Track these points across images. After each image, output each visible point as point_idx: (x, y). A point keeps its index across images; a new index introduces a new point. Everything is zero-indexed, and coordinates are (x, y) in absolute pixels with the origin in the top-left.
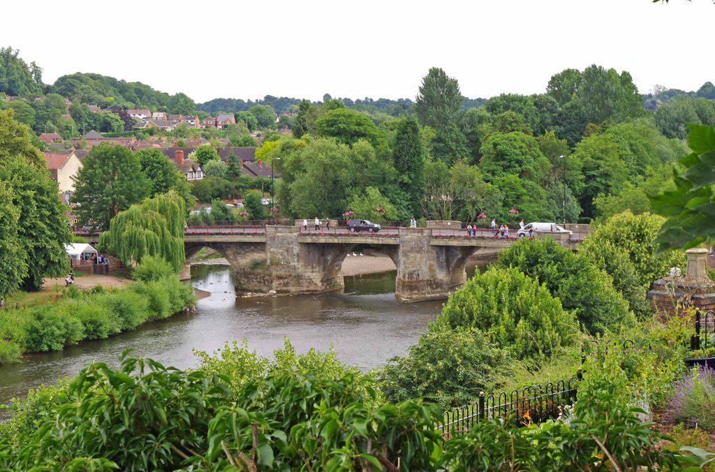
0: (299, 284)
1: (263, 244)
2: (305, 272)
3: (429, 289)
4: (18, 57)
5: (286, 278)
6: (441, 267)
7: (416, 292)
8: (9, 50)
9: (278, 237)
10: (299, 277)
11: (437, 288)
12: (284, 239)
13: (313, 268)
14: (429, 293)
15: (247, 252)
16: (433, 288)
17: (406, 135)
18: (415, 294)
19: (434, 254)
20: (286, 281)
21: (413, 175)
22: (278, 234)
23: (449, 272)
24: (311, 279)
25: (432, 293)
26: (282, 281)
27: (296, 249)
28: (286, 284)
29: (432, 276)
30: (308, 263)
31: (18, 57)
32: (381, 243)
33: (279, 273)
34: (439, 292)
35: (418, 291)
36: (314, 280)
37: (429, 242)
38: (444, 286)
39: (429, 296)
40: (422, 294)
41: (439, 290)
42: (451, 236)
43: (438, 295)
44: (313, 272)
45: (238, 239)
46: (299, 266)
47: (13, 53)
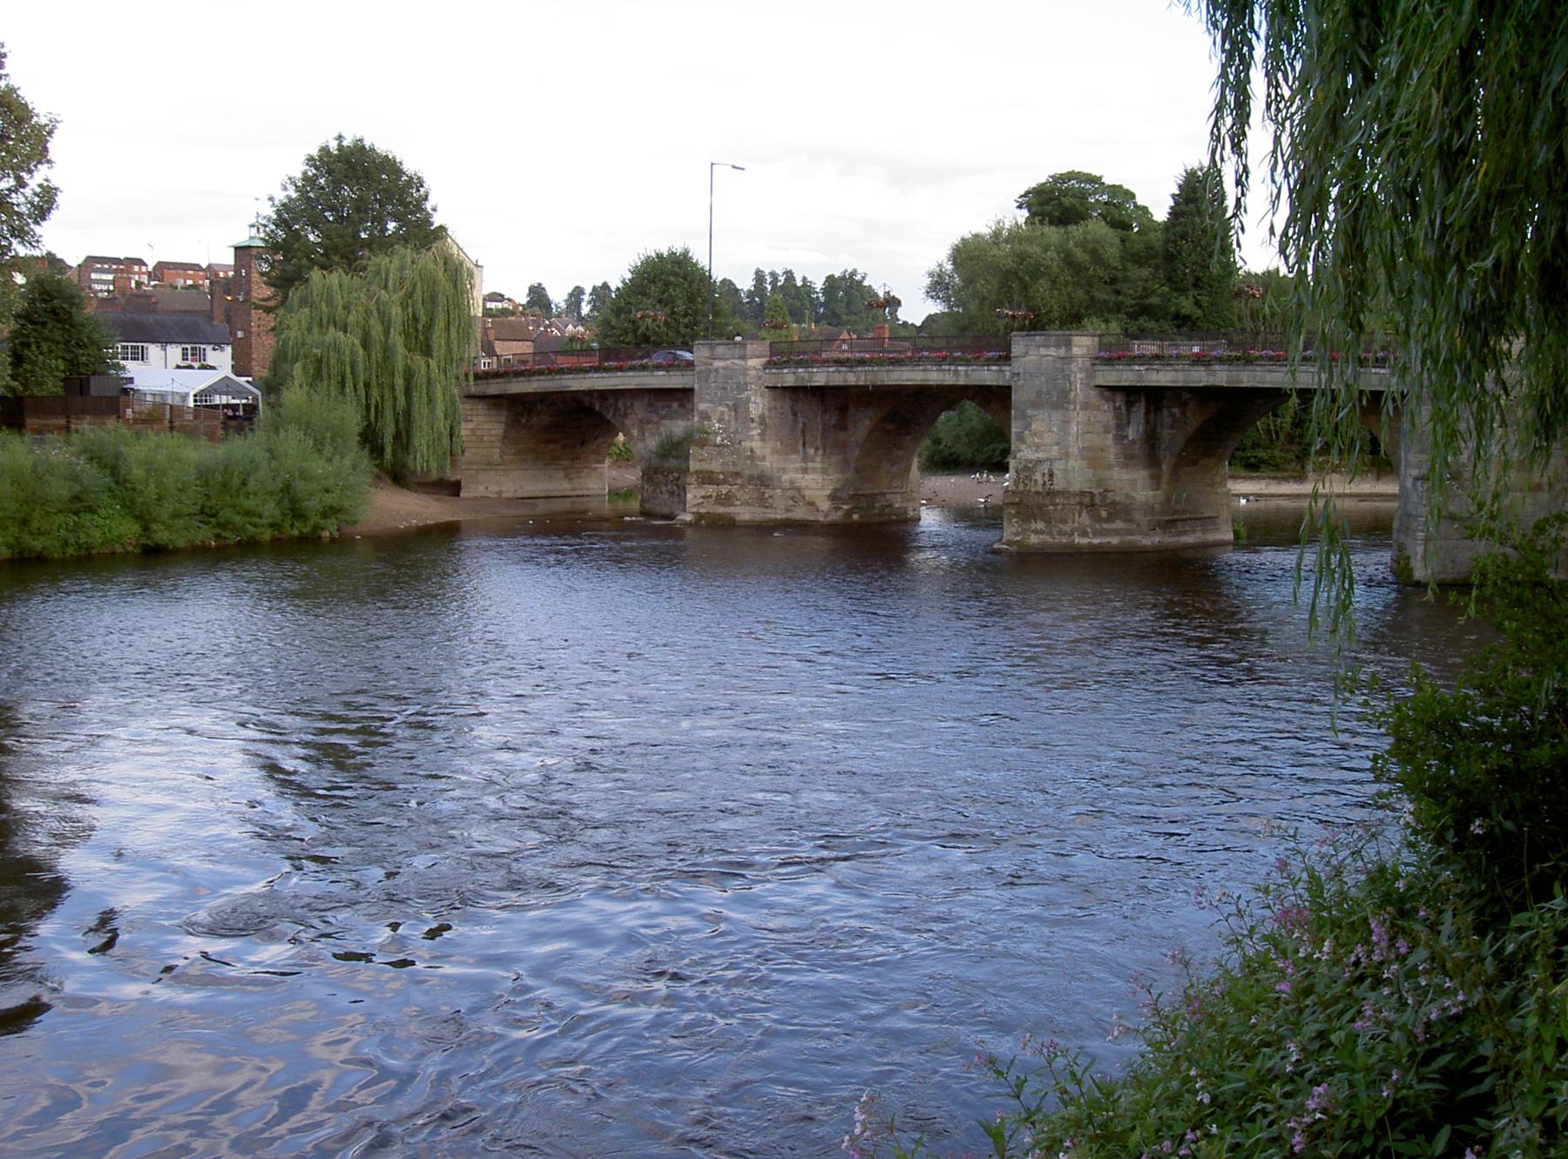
0: (763, 501)
1: (687, 393)
2: (784, 470)
3: (1085, 519)
4: (866, 283)
5: (724, 482)
6: (1128, 459)
7: (1040, 525)
8: (854, 273)
9: (716, 370)
10: (763, 481)
11: (1111, 518)
12: (730, 373)
13: (806, 458)
14: (1084, 534)
15: (664, 418)
16: (1097, 518)
17: (1192, 205)
18: (1037, 532)
19: (1106, 413)
20: (724, 489)
21: (1205, 300)
22: (717, 364)
23: (1156, 480)
24: (798, 489)
25: (1096, 533)
26: (711, 490)
27: (758, 404)
28: (727, 500)
29: (1099, 483)
30: (797, 439)
31: (866, 283)
32: (962, 382)
33: (706, 466)
34: (1116, 532)
35: (1048, 522)
36: (807, 493)
37: (1090, 375)
38: (1138, 516)
39: (1085, 541)
40: (1061, 533)
41: (1119, 525)
42: (1157, 357)
43: (1115, 541)
44: (805, 471)
45: (626, 380)
46: (764, 451)
47: (858, 277)
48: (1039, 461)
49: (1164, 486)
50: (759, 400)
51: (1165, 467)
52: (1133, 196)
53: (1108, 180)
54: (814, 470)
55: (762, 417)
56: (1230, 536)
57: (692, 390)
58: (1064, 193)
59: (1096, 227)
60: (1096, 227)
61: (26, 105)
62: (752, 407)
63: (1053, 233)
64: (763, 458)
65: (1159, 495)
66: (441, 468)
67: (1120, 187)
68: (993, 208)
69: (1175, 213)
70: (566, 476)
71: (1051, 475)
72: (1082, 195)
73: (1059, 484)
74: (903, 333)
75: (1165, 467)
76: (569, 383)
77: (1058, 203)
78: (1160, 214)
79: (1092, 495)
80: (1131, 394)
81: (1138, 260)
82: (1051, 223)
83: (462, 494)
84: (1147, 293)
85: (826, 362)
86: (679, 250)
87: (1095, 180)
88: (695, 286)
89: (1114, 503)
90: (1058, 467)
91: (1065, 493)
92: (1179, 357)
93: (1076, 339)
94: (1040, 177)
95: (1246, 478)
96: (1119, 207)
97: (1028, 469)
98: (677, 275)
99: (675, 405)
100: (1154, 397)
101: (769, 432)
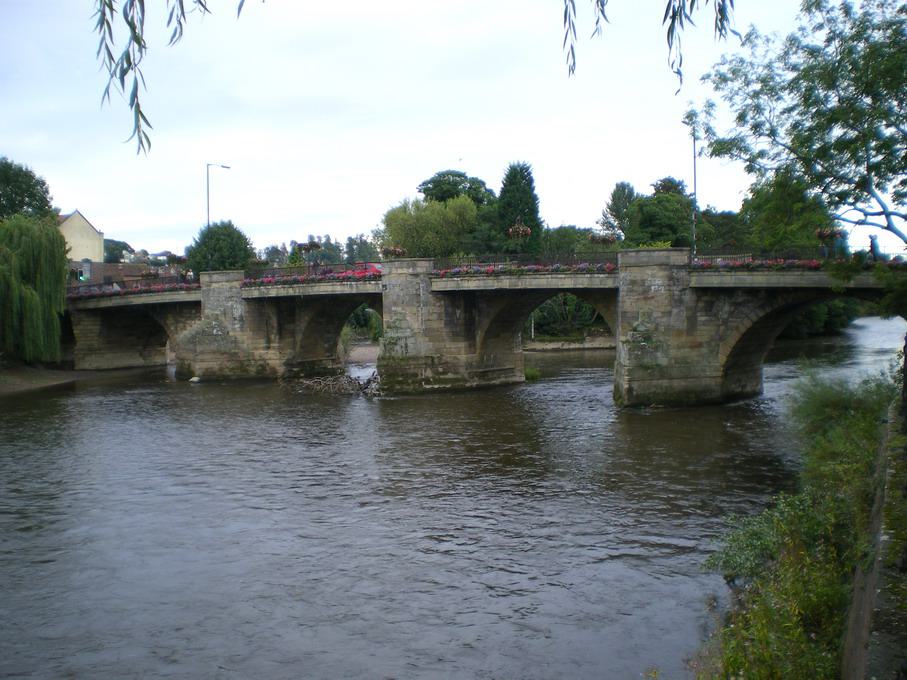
1: (197, 305)
6: (454, 336)
8: (362, 236)
19: (437, 308)
22: (214, 285)
23: (472, 346)
29: (438, 350)
32: (354, 291)
45: (164, 297)
48: (399, 338)
49: (478, 351)
50: (238, 306)
51: (479, 337)
52: (483, 184)
53: (469, 175)
54: (274, 348)
55: (241, 317)
56: (523, 379)
57: (200, 302)
58: (444, 183)
59: (463, 200)
60: (463, 200)
61: (20, 169)
62: (235, 311)
63: (437, 205)
64: (243, 343)
65: (475, 357)
66: (757, 315)
67: (477, 179)
68: (407, 191)
69: (504, 191)
70: (141, 355)
71: (406, 346)
72: (456, 184)
73: (412, 352)
74: (868, 280)
75: (479, 337)
76: (132, 300)
77: (442, 188)
78: (497, 193)
79: (433, 358)
80: (451, 297)
81: (485, 218)
82: (436, 199)
83: (76, 368)
84: (490, 239)
85: (276, 283)
86: (226, 220)
87: (461, 175)
88: (234, 241)
89: (446, 363)
90: (410, 342)
91: (414, 358)
92: (547, 270)
93: (419, 263)
94: (429, 175)
95: (550, 341)
96: (476, 188)
97: (393, 343)
98: (224, 235)
99: (194, 311)
100: (468, 299)
101: (245, 326)
